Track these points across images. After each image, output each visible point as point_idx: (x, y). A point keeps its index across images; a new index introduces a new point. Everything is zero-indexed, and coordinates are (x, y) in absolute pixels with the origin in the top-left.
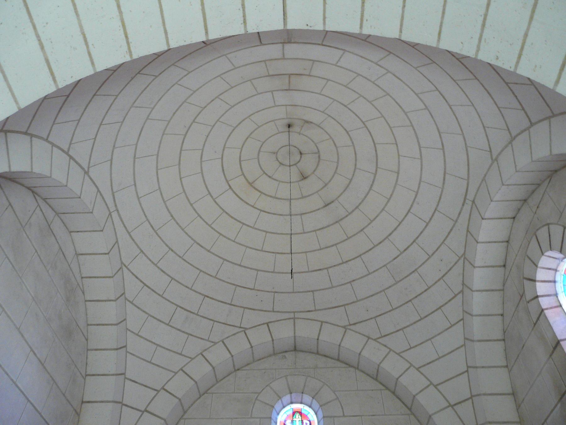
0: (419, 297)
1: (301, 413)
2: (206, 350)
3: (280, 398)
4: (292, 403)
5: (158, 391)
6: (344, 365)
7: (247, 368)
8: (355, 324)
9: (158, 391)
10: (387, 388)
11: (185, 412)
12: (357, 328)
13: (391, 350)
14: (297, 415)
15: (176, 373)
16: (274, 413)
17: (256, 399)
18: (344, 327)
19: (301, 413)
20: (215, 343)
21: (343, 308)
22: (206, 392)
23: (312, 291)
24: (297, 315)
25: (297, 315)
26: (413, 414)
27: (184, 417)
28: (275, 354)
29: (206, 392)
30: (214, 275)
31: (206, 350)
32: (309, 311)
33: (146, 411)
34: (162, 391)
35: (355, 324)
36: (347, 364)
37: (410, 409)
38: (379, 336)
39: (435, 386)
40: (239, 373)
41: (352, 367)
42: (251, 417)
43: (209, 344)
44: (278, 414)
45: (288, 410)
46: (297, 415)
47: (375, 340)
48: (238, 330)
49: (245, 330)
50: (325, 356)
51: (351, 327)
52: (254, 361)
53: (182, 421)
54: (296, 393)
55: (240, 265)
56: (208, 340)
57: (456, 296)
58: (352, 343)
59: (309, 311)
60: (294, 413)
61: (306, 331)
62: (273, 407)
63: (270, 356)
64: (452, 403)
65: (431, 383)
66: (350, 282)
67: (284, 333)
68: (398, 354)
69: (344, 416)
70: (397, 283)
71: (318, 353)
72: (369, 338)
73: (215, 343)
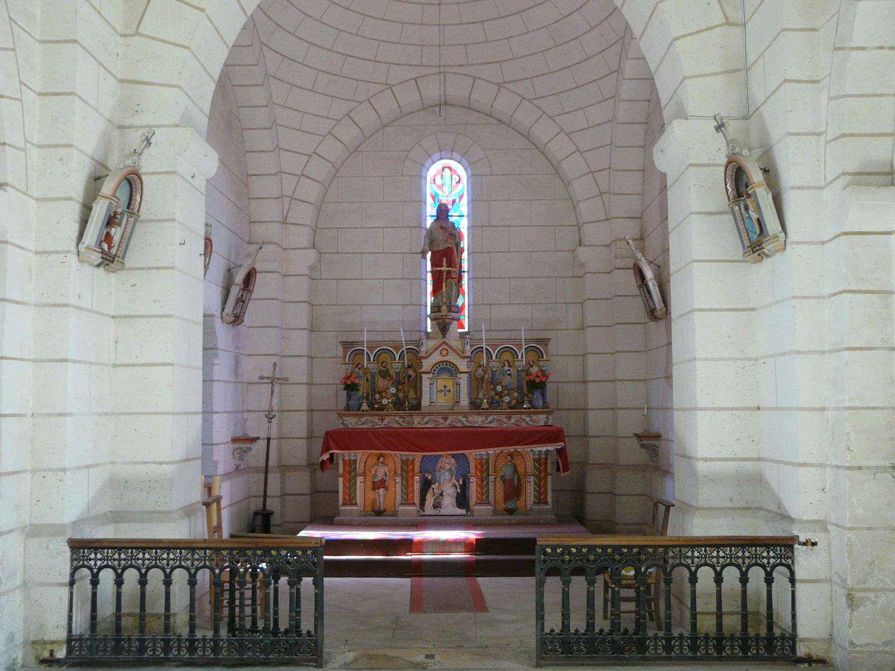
0: (577, 66)
1: (450, 169)
2: (351, 111)
3: (430, 156)
4: (441, 159)
5: (310, 156)
6: (497, 122)
7: (393, 124)
8: (510, 82)
9: (310, 156)
10: (537, 148)
11: (337, 171)
12: (512, 86)
13: (544, 113)
14: (447, 170)
15: (325, 137)
16: (424, 169)
17: (406, 157)
18: (498, 84)
19: (450, 169)
20: (361, 103)
21: (498, 64)
22: (355, 151)
23: (465, 45)
24: (447, 69)
25: (447, 69)
26: (558, 173)
27: (338, 175)
28: (424, 108)
29: (355, 151)
30: (355, 32)
31: (351, 111)
32: (461, 66)
33: (303, 175)
34: (314, 155)
35: (510, 82)
36: (499, 120)
37: (556, 169)
38: (534, 97)
39: (581, 153)
40: (387, 129)
41: (504, 123)
42: (402, 175)
43: (354, 104)
44: (428, 170)
45: (439, 165)
46: (447, 170)
47: (529, 101)
48: (381, 87)
49: (391, 87)
50: (477, 111)
51: (507, 85)
52: (402, 117)
53: (336, 179)
54: (445, 151)
55: (383, 19)
56: (354, 101)
57: (611, 73)
58: (505, 104)
59: (461, 66)
60: (443, 168)
61: (457, 89)
62: (423, 165)
63: (419, 110)
64: (593, 170)
65: (578, 150)
66: (507, 38)
67: (432, 91)
68: (551, 118)
69: (492, 175)
70: (557, 46)
71: (470, 108)
72: (523, 98)
73: (361, 103)
